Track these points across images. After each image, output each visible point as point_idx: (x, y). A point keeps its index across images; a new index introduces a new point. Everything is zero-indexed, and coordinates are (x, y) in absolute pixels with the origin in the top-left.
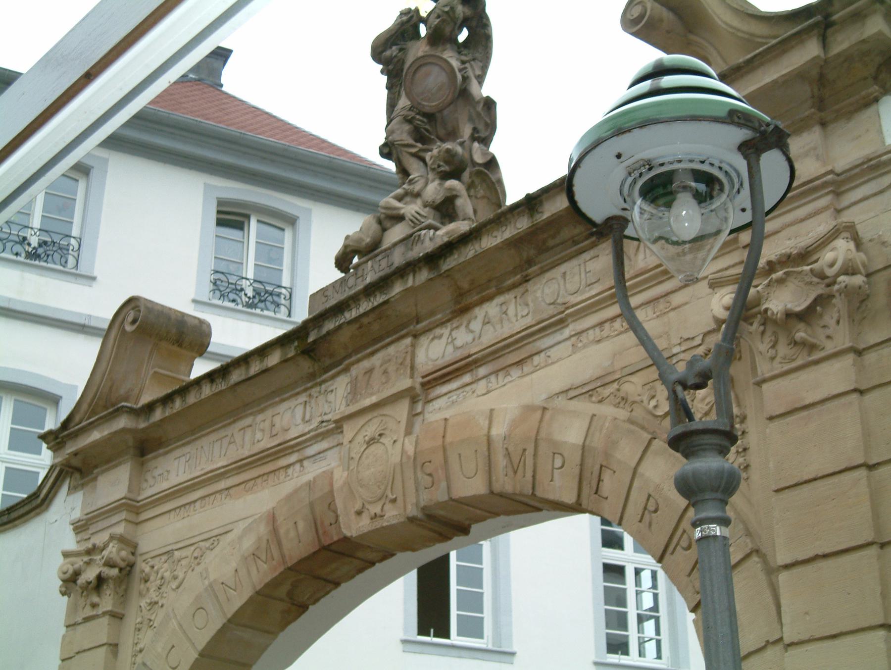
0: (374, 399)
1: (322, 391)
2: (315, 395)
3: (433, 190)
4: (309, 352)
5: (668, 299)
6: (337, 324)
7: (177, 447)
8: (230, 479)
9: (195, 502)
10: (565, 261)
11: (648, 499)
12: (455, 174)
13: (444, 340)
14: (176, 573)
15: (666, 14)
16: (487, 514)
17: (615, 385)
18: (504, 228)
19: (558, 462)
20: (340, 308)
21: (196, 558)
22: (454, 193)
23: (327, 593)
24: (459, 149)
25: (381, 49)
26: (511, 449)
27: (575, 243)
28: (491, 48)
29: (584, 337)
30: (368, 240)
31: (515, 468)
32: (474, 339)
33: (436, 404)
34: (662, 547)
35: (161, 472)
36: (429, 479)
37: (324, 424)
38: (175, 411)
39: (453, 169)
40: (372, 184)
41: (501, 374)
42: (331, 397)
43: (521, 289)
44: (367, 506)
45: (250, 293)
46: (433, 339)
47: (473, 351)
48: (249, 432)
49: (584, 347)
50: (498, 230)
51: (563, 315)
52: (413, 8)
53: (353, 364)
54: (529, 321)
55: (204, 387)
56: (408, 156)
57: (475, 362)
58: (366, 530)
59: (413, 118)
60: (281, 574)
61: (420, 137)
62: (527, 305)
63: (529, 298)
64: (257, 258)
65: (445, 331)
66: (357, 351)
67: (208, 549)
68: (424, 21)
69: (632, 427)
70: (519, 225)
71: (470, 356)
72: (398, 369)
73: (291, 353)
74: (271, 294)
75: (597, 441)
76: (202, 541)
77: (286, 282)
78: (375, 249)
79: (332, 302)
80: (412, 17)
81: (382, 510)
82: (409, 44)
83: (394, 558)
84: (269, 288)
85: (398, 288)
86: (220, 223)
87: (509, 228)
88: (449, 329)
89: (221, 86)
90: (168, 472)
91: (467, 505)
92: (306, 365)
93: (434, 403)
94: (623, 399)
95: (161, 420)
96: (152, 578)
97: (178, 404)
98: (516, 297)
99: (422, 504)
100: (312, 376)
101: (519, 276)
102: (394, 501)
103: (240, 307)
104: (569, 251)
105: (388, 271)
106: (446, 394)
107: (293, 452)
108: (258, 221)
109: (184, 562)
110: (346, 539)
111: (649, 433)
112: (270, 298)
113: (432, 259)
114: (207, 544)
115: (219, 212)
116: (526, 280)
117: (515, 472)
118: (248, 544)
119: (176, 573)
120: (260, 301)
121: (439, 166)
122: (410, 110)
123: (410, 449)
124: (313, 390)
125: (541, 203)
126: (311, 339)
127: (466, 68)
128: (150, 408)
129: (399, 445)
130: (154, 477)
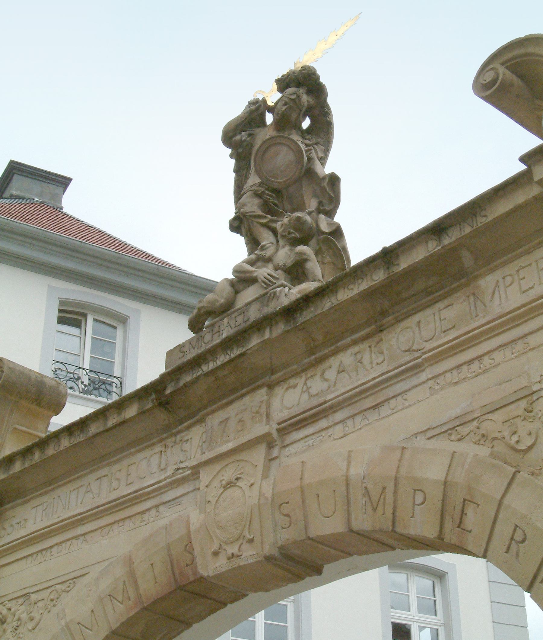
0: (231, 445)
1: (178, 441)
2: (170, 445)
3: (284, 255)
4: (165, 403)
5: (526, 340)
6: (194, 376)
7: (37, 497)
8: (87, 525)
9: (52, 547)
10: (420, 311)
11: (515, 530)
12: (304, 241)
13: (299, 389)
14: (32, 614)
15: (515, 80)
16: (342, 554)
17: (475, 423)
18: (360, 281)
19: (419, 498)
20: (197, 362)
21: (52, 600)
22: (305, 257)
23: (179, 633)
24: (308, 219)
25: (231, 134)
26: (370, 487)
27: (430, 294)
28: (332, 134)
29: (441, 380)
30: (222, 301)
31: (375, 504)
32: (329, 387)
33: (292, 449)
34: (531, 576)
35: (18, 521)
36: (287, 519)
37: (181, 471)
38: (34, 463)
39: (302, 235)
40: (194, 290)
41: (358, 419)
42: (186, 446)
43: (376, 339)
44: (224, 547)
45: (86, 382)
46: (287, 389)
47: (329, 397)
48: (105, 480)
49: (442, 389)
50: (354, 283)
51: (420, 360)
52: (261, 99)
53: (208, 414)
54: (384, 368)
55: (63, 440)
56: (259, 226)
57: (331, 407)
58: (223, 570)
59: (263, 193)
60: (137, 613)
61: (268, 208)
62: (382, 353)
63: (384, 347)
64: (93, 351)
65: (300, 381)
66: (212, 402)
67: (64, 591)
68: (271, 109)
69: (496, 462)
70: (375, 277)
71: (325, 402)
72: (253, 417)
73: (149, 406)
74: (104, 383)
75: (459, 476)
76: (59, 584)
77: (117, 372)
78: (228, 310)
79: (189, 357)
80: (260, 106)
81: (239, 550)
82: (257, 130)
83: (245, 599)
84: (103, 378)
85: (254, 341)
86: (61, 321)
87: (365, 280)
88: (304, 378)
89: (62, 208)
90: (26, 520)
91: (323, 544)
92: (161, 417)
93: (290, 448)
94: (483, 436)
95: (21, 472)
96: (9, 620)
97: (37, 456)
98: (370, 347)
99: (280, 543)
100: (167, 428)
101: (373, 327)
102: (251, 541)
103: (77, 393)
104: (424, 301)
105: (243, 326)
106: (302, 439)
107: (149, 498)
108: (95, 320)
109: (40, 604)
110: (202, 579)
111: (512, 466)
112: (103, 386)
113: (289, 312)
114: (63, 587)
115: (60, 311)
116: (380, 330)
117: (375, 510)
118: (105, 584)
119: (32, 614)
120: (95, 389)
121: (289, 233)
122: (260, 186)
123: (268, 492)
124: (169, 440)
125: (397, 256)
126: (168, 392)
127: (311, 150)
128: (10, 460)
129: (256, 488)
130: (12, 526)
